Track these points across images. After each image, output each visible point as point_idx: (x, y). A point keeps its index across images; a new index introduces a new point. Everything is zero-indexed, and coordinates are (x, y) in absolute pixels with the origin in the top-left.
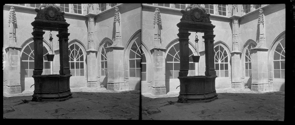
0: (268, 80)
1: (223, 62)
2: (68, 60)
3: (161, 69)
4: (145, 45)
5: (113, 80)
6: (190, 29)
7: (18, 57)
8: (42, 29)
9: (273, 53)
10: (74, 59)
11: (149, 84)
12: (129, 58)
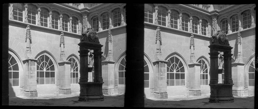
0: (243, 88)
1: (179, 72)
2: (125, 72)
3: (34, 76)
4: (20, 59)
5: (237, 89)
6: (219, 50)
8: (218, 50)
9: (248, 67)
10: (44, 69)
11: (21, 88)
12: (248, 71)
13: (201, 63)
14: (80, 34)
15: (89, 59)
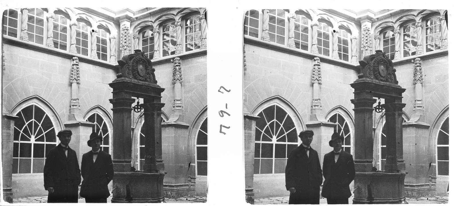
7: (253, 135)
13: (335, 122)
14: (356, 64)
15: (377, 115)
